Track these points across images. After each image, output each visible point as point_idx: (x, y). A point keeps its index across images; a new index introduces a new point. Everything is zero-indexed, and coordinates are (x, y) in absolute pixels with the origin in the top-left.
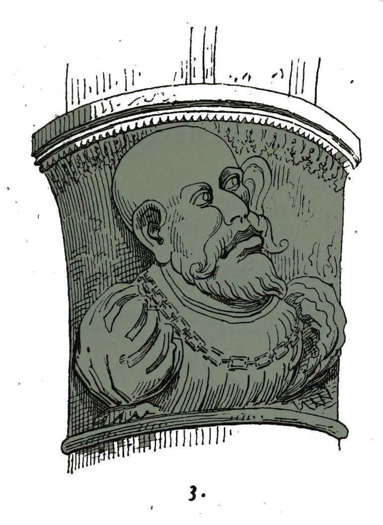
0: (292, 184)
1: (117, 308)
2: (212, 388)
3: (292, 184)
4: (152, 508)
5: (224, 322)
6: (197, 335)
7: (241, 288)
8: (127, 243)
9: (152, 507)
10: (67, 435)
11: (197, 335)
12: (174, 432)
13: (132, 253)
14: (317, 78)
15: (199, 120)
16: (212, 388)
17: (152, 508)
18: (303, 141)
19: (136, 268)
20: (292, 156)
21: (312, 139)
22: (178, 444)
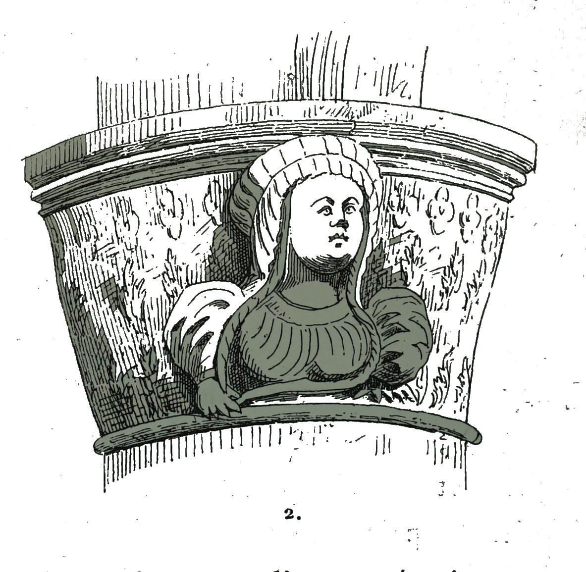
0: (332, 153)
1: (245, 226)
2: (278, 307)
3: (332, 153)
4: (504, 390)
5: (423, 330)
6: (116, 340)
7: (412, 369)
8: (180, 387)
9: (472, 234)
10: (232, 314)
11: (116, 340)
12: (154, 445)
13: (179, 389)
14: (478, 334)
15: (243, 170)
16: (278, 307)
17: (504, 390)
18: (351, 165)
19: (176, 393)
20: (344, 101)
21: (342, 235)
22: (270, 358)
